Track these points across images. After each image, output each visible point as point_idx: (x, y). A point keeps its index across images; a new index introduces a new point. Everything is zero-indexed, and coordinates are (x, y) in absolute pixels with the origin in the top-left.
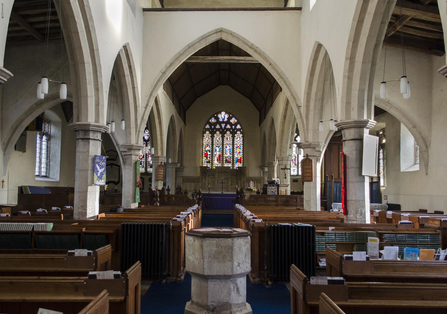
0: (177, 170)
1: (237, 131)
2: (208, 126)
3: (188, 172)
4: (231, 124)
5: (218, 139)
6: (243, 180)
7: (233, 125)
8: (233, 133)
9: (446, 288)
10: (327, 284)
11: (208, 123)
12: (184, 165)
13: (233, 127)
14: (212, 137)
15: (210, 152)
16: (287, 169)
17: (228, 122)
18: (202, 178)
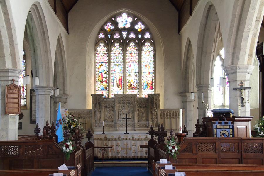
0: (54, 100)
1: (145, 42)
2: (102, 36)
3: (73, 104)
4: (136, 32)
5: (117, 54)
6: (155, 114)
7: (140, 33)
8: (140, 44)
9: (2, 74)
10: (172, 169)
11: (102, 30)
12: (68, 92)
13: (140, 36)
14: (109, 51)
15: (106, 73)
16: (245, 89)
17: (132, 29)
18: (95, 112)
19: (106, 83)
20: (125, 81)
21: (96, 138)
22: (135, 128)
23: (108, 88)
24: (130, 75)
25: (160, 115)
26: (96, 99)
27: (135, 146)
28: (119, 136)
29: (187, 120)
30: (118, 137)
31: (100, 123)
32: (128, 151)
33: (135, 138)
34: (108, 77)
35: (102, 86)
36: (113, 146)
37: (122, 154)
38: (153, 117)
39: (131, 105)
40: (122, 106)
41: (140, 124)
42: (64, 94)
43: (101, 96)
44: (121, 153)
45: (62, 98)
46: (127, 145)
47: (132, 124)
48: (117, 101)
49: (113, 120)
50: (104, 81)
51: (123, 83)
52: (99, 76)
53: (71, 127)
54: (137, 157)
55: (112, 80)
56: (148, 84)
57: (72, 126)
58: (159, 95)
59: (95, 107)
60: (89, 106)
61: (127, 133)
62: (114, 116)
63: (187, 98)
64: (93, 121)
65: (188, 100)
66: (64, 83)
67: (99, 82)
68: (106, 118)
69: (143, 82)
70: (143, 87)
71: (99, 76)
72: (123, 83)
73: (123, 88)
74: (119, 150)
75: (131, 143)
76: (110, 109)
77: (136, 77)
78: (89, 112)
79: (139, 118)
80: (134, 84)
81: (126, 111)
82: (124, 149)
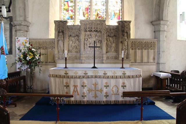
6: (126, 44)
12: (30, 19)
18: (58, 41)
19: (72, 12)
20: (91, 10)
21: (53, 75)
22: (103, 60)
23: (73, 17)
24: (96, 3)
25: (131, 46)
26: (60, 26)
27: (108, 86)
28: (85, 71)
29: (159, 51)
30: (84, 74)
31: (63, 54)
32: (98, 93)
33: (89, 74)
34: (74, 6)
35: (67, 15)
36: (77, 86)
37: (89, 98)
38: (123, 47)
39: (99, 33)
40: (89, 34)
41: (109, 55)
42: (25, 20)
43: (65, 23)
44: (87, 96)
45: (22, 26)
46: (96, 84)
47: (100, 55)
48: (82, 28)
49: (79, 51)
50: (69, 10)
51: (90, 12)
52: (65, 5)
53: (27, 59)
54: (111, 102)
55: (78, 9)
56: (115, 14)
57: (27, 57)
58: (130, 22)
59: (58, 36)
60: (52, 35)
61: (94, 67)
62: (79, 46)
63: (160, 26)
64: (56, 52)
65: (161, 29)
66: (25, 9)
67: (65, 11)
68: (71, 49)
69: (109, 11)
70: (110, 17)
71: (65, 5)
72: (90, 12)
73: (89, 17)
74: (85, 92)
75: (102, 83)
76: (75, 38)
77: (103, 6)
78: (52, 41)
79: (107, 49)
80: (101, 14)
81: (91, 40)
82: (92, 90)
